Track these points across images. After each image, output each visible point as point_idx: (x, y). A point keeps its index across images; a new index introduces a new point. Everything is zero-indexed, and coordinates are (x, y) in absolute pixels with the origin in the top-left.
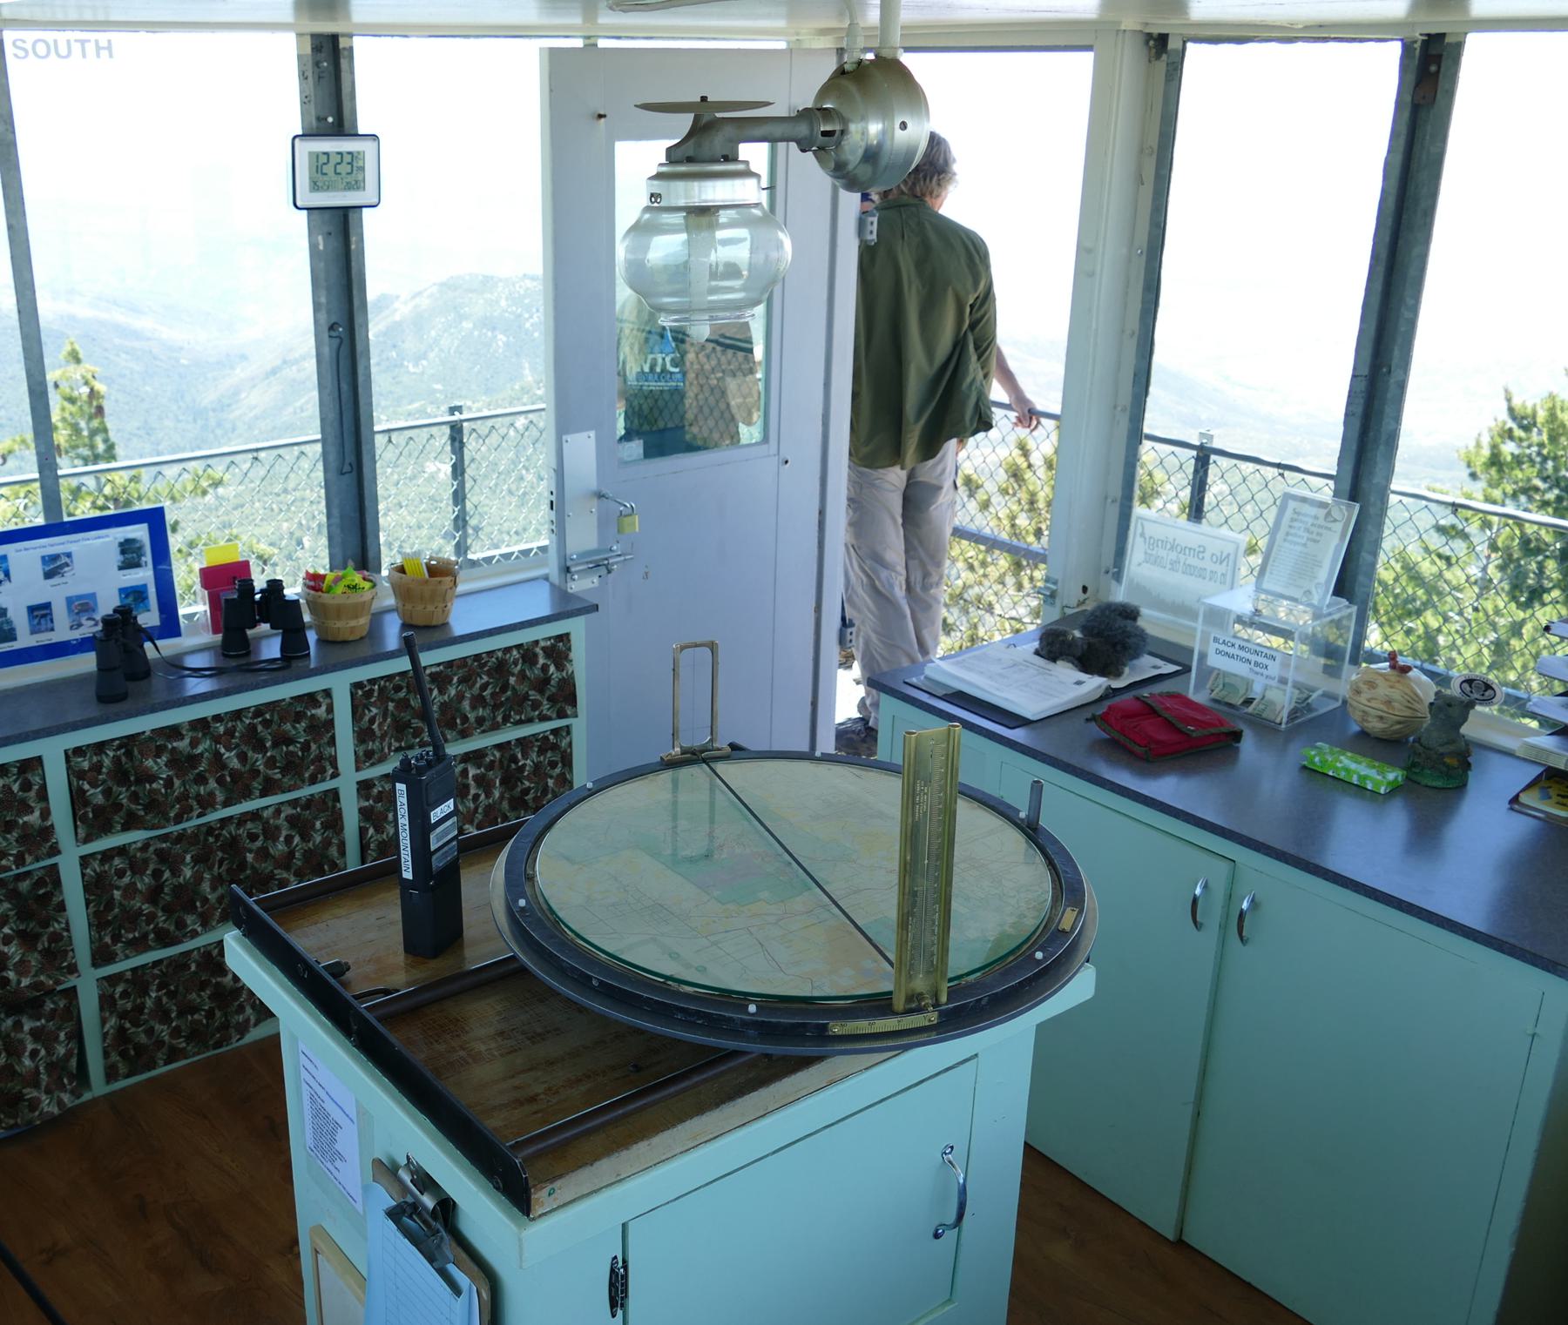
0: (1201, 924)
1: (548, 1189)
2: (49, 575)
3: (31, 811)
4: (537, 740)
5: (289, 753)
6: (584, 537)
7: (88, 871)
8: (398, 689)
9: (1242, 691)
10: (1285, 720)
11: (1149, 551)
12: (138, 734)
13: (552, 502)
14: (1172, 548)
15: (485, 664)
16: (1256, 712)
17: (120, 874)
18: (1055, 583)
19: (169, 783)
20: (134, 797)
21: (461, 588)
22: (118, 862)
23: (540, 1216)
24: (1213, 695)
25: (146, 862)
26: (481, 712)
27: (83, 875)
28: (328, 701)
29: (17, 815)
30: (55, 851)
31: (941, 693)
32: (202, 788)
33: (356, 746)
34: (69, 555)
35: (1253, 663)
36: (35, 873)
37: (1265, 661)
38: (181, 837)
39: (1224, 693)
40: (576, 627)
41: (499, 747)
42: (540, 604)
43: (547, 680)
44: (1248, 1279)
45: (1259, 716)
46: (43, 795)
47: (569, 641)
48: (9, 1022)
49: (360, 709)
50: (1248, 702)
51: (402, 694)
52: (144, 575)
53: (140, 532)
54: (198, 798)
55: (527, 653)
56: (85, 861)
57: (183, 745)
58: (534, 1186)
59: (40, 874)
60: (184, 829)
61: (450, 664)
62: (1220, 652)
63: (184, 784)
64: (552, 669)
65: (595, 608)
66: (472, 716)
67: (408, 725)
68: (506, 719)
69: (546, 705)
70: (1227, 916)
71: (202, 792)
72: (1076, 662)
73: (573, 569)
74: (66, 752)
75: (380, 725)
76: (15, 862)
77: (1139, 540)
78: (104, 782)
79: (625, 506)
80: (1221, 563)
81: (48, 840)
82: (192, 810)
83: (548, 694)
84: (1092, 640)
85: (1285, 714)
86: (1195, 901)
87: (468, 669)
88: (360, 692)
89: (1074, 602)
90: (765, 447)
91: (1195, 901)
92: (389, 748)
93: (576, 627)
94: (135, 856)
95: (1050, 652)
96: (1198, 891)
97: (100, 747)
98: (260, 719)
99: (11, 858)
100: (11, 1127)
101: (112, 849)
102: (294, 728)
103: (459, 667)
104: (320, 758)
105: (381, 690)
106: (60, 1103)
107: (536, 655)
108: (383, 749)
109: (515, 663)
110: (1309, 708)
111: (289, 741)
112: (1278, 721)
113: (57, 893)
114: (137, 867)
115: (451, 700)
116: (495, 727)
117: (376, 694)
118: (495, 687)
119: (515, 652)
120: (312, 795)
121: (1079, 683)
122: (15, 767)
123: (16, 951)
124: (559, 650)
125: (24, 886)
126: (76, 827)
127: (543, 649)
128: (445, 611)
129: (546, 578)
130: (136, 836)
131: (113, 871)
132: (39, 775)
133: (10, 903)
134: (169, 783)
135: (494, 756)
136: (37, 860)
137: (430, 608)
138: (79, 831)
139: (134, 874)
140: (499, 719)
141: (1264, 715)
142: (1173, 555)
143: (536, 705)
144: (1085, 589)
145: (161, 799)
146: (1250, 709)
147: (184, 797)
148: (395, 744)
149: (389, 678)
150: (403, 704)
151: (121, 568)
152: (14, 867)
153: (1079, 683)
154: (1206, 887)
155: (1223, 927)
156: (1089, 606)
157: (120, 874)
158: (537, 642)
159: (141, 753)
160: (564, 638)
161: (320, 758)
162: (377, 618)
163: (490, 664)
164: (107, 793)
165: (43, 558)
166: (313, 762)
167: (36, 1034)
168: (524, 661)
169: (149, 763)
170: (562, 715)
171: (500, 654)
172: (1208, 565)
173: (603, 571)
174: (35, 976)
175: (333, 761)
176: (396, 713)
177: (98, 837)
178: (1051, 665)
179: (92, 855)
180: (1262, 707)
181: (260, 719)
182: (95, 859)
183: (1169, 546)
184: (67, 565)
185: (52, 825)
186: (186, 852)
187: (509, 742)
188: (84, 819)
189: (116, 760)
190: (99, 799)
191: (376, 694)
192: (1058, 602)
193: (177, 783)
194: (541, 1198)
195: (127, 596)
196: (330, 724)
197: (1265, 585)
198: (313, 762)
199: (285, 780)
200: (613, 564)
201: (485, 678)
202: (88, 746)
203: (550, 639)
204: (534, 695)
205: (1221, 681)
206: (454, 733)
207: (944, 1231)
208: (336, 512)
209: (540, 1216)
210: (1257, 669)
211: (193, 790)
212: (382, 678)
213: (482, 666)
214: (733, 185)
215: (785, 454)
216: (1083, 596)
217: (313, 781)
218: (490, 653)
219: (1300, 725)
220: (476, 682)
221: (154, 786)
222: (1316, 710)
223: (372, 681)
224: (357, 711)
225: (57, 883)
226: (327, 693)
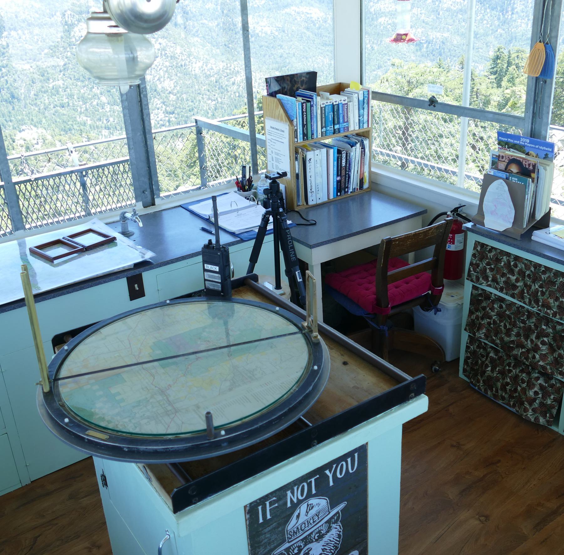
25: (536, 345)
29: (561, 296)
32: (514, 333)
48: (536, 375)
71: (512, 333)
76: (552, 314)
98: (492, 322)
99: (552, 312)
100: (517, 411)
102: (483, 333)
106: (537, 419)
123: (545, 350)
133: (553, 331)
152: (551, 315)
167: (542, 387)
174: (546, 364)
181: (492, 322)
211: (515, 330)
214: (510, 222)
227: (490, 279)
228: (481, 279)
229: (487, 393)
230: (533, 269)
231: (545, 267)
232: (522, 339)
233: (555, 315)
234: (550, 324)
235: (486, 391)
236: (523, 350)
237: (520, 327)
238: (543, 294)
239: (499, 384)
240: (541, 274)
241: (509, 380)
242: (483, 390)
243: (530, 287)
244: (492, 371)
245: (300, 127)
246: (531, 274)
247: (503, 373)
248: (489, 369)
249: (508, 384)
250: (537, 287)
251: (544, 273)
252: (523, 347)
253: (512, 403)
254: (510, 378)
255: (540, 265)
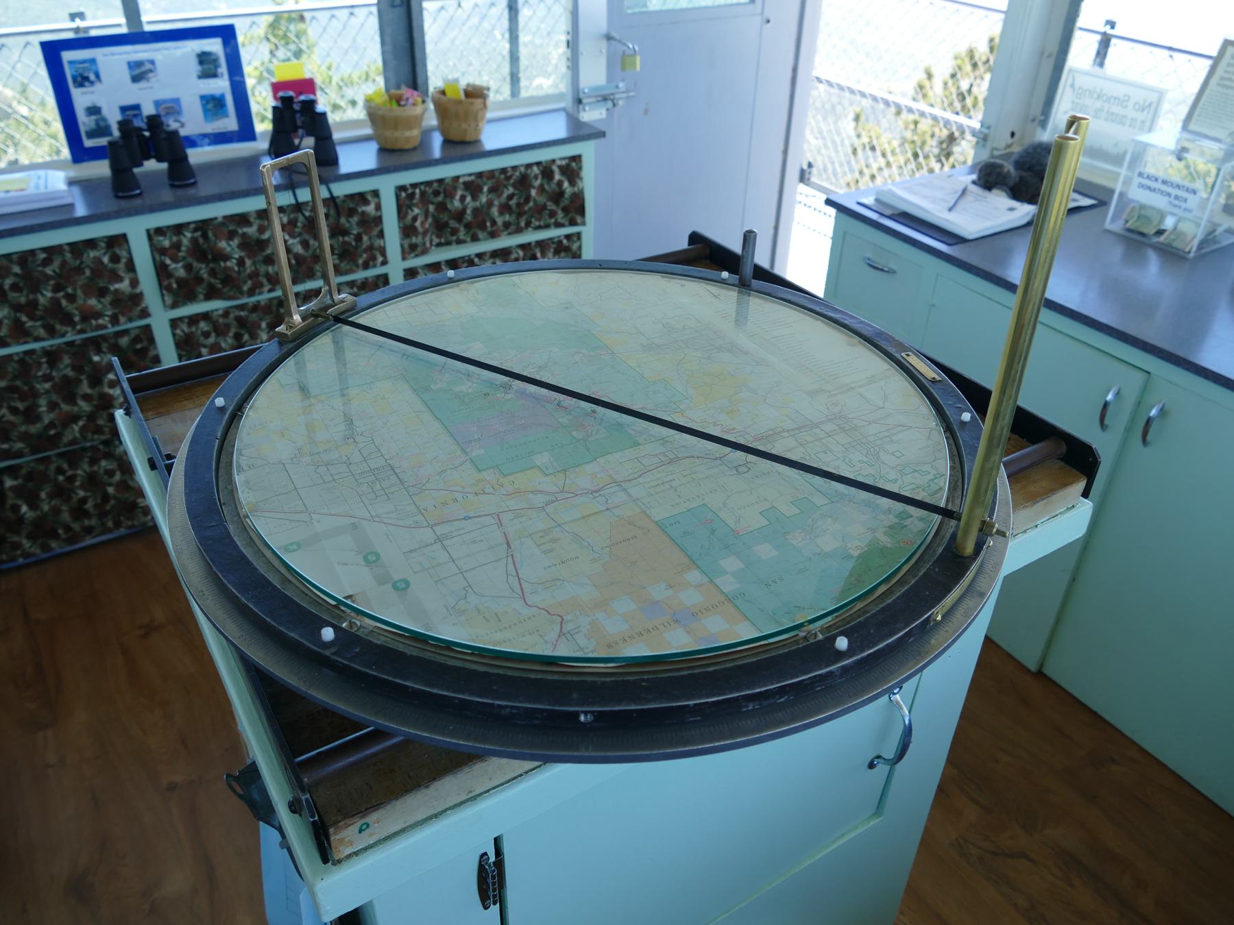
0: (1107, 426)
1: (358, 825)
2: (136, 79)
3: (120, 279)
4: (553, 243)
5: (344, 243)
6: (594, 74)
7: (178, 331)
8: (436, 193)
9: (1155, 223)
10: (1194, 249)
11: (1076, 100)
12: (211, 220)
13: (568, 42)
14: (1099, 97)
15: (510, 177)
16: (1166, 242)
17: (206, 335)
18: (988, 128)
19: (241, 262)
20: (213, 273)
21: (490, 115)
22: (203, 325)
23: (349, 856)
24: (1128, 225)
25: (227, 326)
26: (507, 217)
27: (174, 335)
28: (376, 200)
30: (145, 314)
31: (888, 212)
33: (402, 239)
34: (152, 62)
35: (1173, 196)
36: (133, 331)
37: (1185, 195)
38: (256, 308)
39: (1138, 224)
40: (586, 150)
41: (522, 247)
42: (557, 128)
43: (561, 194)
44: (1094, 708)
45: (1169, 245)
46: (131, 267)
47: (580, 161)
49: (404, 209)
50: (1160, 232)
51: (440, 198)
52: (221, 85)
53: (214, 45)
54: (267, 275)
55: (546, 170)
56: (174, 323)
57: (251, 231)
58: (336, 823)
59: (137, 332)
60: (259, 302)
61: (480, 175)
62: (1143, 186)
63: (254, 264)
64: (566, 184)
65: (602, 134)
66: (500, 221)
67: (446, 225)
68: (528, 224)
69: (560, 216)
70: (1133, 420)
72: (1009, 192)
73: (584, 101)
74: (148, 231)
75: (423, 223)
77: (1068, 89)
78: (184, 258)
79: (628, 47)
80: (1143, 110)
81: (137, 304)
82: (262, 285)
83: (562, 205)
84: (1023, 174)
85: (1196, 243)
86: (1106, 405)
87: (498, 179)
88: (403, 194)
89: (1002, 145)
90: (752, 6)
91: (1106, 405)
92: (431, 244)
93: (586, 150)
94: (217, 321)
95: (987, 182)
96: (1110, 397)
97: (179, 229)
99: (107, 318)
100: (129, 527)
101: (198, 315)
103: (488, 178)
104: (371, 248)
105: (423, 194)
107: (552, 172)
108: (424, 244)
109: (536, 177)
110: (1215, 241)
111: (345, 232)
112: (1187, 250)
113: (151, 348)
114: (220, 330)
115: (482, 206)
116: (519, 230)
117: (417, 196)
118: (520, 198)
119: (535, 168)
120: (366, 279)
121: (1011, 209)
122: (102, 241)
124: (572, 169)
125: (124, 341)
126: (163, 295)
127: (560, 167)
128: (477, 130)
129: (564, 109)
130: (217, 305)
131: (199, 332)
132: (125, 250)
134: (241, 262)
135: (518, 253)
136: (130, 320)
137: (464, 126)
138: (166, 298)
139: (218, 335)
140: (523, 224)
141: (1175, 244)
142: (1098, 104)
143: (552, 214)
144: (1013, 134)
145: (234, 275)
146: (1162, 239)
147: (254, 275)
148: (436, 240)
149: (429, 183)
150: (442, 207)
151: (200, 77)
153: (1011, 209)
154: (1118, 394)
155: (1128, 430)
156: (1017, 149)
157: (206, 335)
158: (553, 161)
159: (215, 235)
160: (577, 159)
161: (371, 248)
162: (426, 134)
163: (514, 177)
164: (188, 268)
165: (129, 64)
166: (365, 251)
168: (543, 177)
169: (223, 244)
170: (573, 223)
171: (522, 169)
172: (1130, 113)
173: (610, 104)
175: (383, 251)
176: (436, 214)
177: (184, 304)
178: (986, 193)
179: (181, 319)
180: (1173, 237)
182: (183, 322)
183: (1095, 96)
184: (151, 71)
185: (141, 294)
186: (261, 319)
187: (530, 244)
188: (169, 288)
189: (194, 241)
190: (181, 273)
191: (417, 196)
192: (989, 145)
193: (248, 262)
194: (347, 837)
195: (207, 103)
196: (379, 220)
197: (1192, 127)
198: (365, 251)
199: (342, 265)
200: (619, 99)
201: (511, 190)
202: (168, 227)
203: (564, 159)
204: (551, 206)
205: (1136, 214)
206: (485, 234)
207: (878, 763)
208: (388, 39)
209: (349, 856)
210: (1176, 202)
211: (43, 402)
212: (422, 183)
213: (508, 178)
215: (767, 14)
216: (1010, 140)
217: (366, 266)
218: (514, 168)
219: (1204, 255)
220: (503, 192)
221: (228, 264)
222: (1218, 242)
223: (414, 186)
224: (402, 209)
225: (151, 340)
226: (376, 193)
227: (77, 319)
228: (58, 327)
229: (50, 549)
230: (17, 269)
231: (44, 250)
232: (65, 407)
233: (115, 320)
234: (104, 346)
235: (45, 548)
236: (81, 423)
237: (47, 392)
238: (71, 298)
239: (66, 516)
240: (40, 269)
241: (81, 493)
242: (38, 551)
243: (34, 304)
244: (33, 506)
245: (1073, 156)
246: (18, 280)
247: (61, 493)
248: (24, 509)
249: (84, 501)
250: (49, 295)
251: (47, 262)
252: (74, 418)
253: (110, 524)
254: (82, 487)
255: (32, 252)
